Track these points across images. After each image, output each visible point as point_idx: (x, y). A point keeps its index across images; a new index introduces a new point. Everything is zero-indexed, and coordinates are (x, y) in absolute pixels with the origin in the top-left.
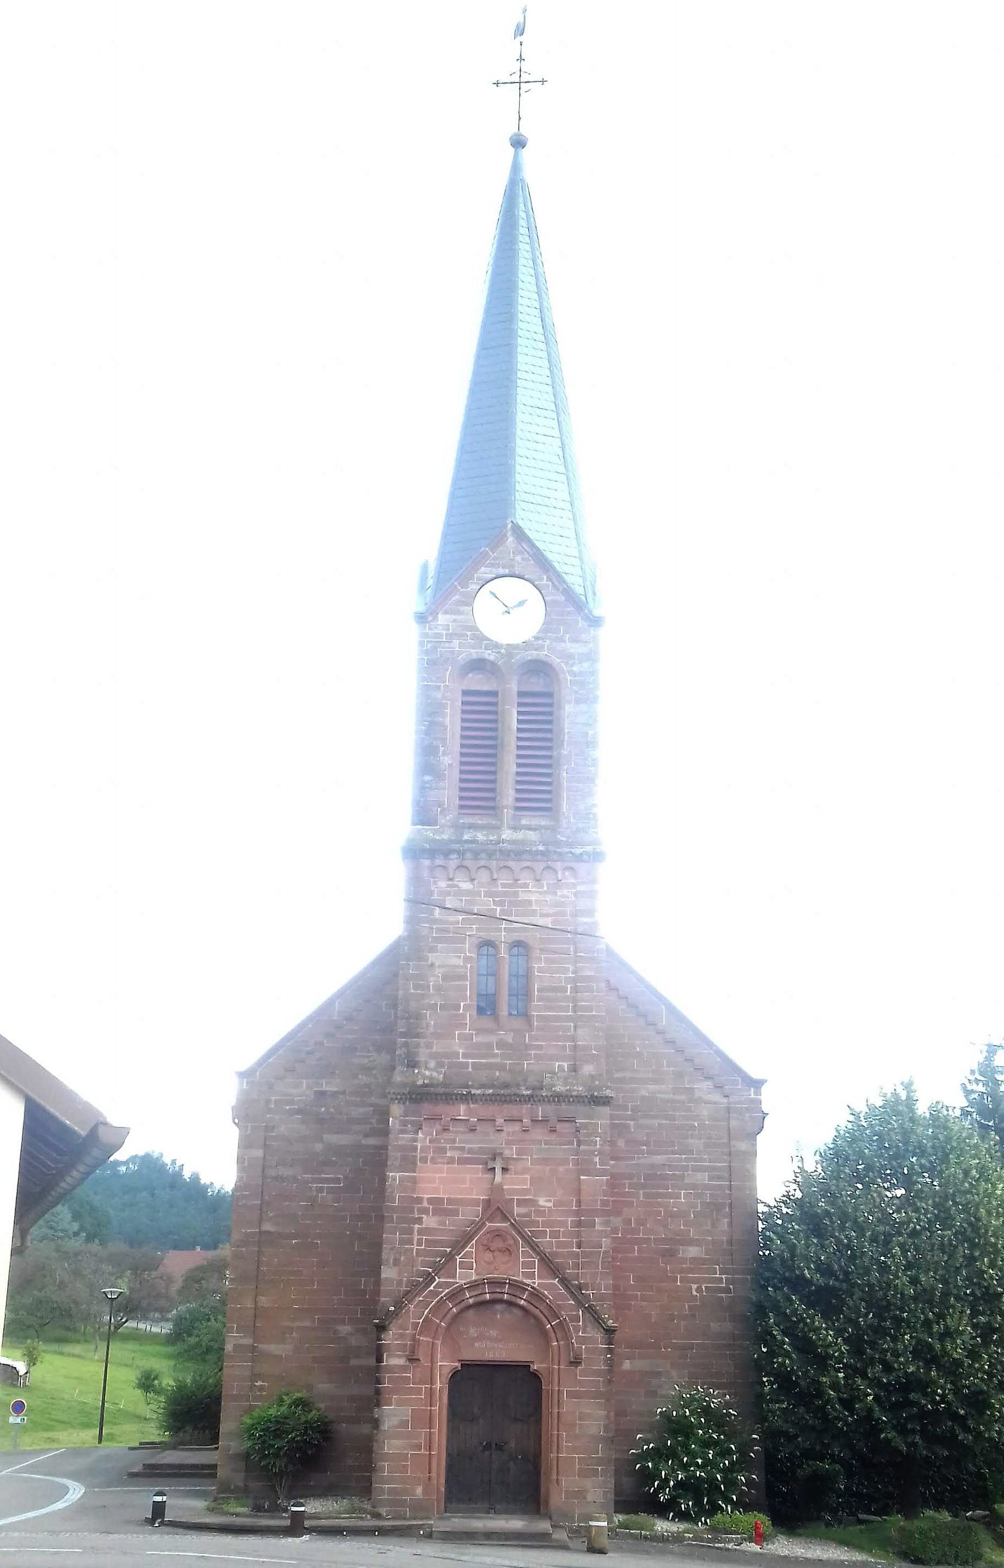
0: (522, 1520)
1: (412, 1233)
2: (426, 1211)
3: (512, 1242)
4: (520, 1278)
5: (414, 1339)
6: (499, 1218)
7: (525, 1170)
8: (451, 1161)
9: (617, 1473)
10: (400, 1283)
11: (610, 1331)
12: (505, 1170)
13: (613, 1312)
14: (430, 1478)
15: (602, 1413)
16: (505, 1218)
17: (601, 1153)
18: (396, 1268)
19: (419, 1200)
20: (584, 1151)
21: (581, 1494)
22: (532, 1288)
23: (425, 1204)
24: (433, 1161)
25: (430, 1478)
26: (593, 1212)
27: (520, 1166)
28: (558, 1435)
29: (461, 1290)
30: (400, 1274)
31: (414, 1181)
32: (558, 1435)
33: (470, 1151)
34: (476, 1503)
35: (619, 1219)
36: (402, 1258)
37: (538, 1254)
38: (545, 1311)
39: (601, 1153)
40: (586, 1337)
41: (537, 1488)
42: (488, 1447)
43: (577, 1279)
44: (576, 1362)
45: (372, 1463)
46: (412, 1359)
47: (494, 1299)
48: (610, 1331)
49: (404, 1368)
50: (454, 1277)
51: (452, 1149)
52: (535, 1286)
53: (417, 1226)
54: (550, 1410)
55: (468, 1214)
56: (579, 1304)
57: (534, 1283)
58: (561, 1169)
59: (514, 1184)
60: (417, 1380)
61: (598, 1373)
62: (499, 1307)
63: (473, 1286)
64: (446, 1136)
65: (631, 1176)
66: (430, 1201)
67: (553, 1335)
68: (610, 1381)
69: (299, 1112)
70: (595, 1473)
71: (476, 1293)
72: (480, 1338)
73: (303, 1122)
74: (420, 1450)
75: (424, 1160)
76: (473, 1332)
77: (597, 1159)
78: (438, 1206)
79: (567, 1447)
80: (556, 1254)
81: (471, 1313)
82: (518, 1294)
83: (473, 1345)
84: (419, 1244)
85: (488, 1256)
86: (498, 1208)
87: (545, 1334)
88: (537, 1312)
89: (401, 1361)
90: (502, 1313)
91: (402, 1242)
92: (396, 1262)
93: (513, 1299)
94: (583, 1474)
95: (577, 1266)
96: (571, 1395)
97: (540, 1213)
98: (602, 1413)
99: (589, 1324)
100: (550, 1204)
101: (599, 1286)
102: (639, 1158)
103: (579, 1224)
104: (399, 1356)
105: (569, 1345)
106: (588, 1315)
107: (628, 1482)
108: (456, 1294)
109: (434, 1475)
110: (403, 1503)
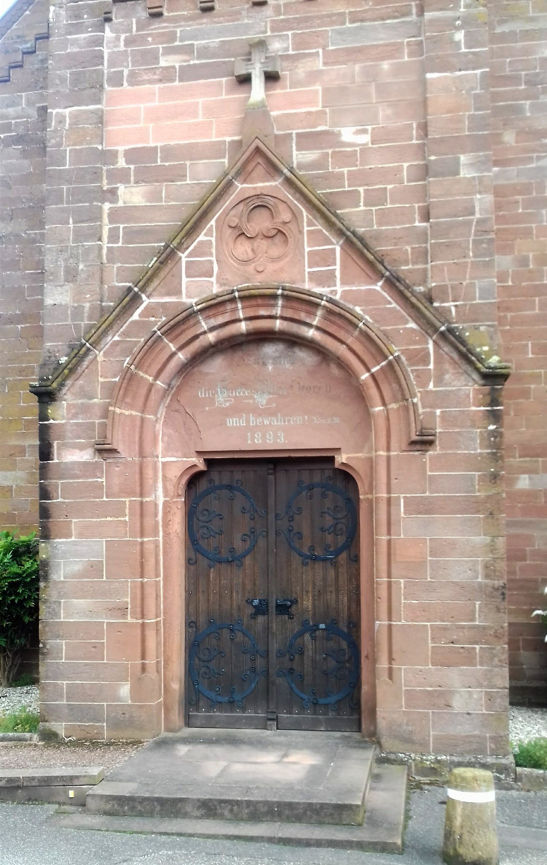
0: (315, 749)
1: (100, 218)
2: (122, 176)
3: (286, 216)
4: (307, 286)
5: (106, 414)
6: (260, 170)
7: (314, 76)
8: (167, 75)
9: (513, 645)
10: (77, 312)
11: (494, 378)
12: (271, 78)
13: (499, 339)
14: (144, 668)
15: (480, 540)
16: (273, 169)
17: (467, 22)
18: (69, 286)
19: (111, 156)
20: (432, 21)
21: (440, 698)
22: (330, 301)
23: (121, 163)
24: (134, 79)
25: (144, 668)
26: (457, 144)
27: (302, 69)
28: (389, 584)
29: (188, 317)
30: (78, 295)
31: (100, 120)
32: (389, 584)
33: (204, 52)
34: (244, 710)
35: (509, 258)
36: (81, 266)
37: (340, 233)
38: (357, 347)
39: (467, 22)
40: (447, 394)
41: (356, 684)
42: (261, 609)
43: (424, 281)
44: (423, 443)
45: (38, 642)
46: (105, 451)
47: (256, 331)
48: (494, 378)
49: (87, 468)
50: (178, 292)
51: (169, 51)
52: (337, 297)
53: (107, 206)
54: (375, 538)
55: (204, 173)
56: (428, 326)
57: (335, 292)
58: (386, 65)
59: (291, 106)
60: (116, 489)
61: (470, 462)
62: (270, 350)
63: (213, 306)
64: (158, 27)
65: (525, 189)
66: (132, 155)
67: (373, 392)
68: (495, 477)
69: (19, 140)
70: (469, 658)
71: (221, 320)
72: (236, 410)
73: (25, 154)
74: (124, 616)
75: (116, 79)
76: (222, 399)
77: (460, 36)
78: (147, 165)
79: (409, 606)
80: (378, 236)
81: (217, 366)
82: (303, 316)
83: (223, 424)
84: (113, 236)
85: (243, 249)
86: (258, 150)
87: (359, 395)
88: (341, 350)
89: (85, 456)
90: (275, 360)
91: (79, 236)
92: (71, 275)
93: (294, 328)
94: (443, 660)
95: (422, 255)
96: (421, 507)
97: (347, 158)
98: (480, 540)
99: (447, 366)
100: (365, 139)
101: (468, 287)
102: (539, 158)
103: (425, 171)
104: (82, 447)
105: (407, 408)
106: (447, 349)
107: (529, 659)
108: (181, 322)
109: (151, 662)
110: (95, 715)
